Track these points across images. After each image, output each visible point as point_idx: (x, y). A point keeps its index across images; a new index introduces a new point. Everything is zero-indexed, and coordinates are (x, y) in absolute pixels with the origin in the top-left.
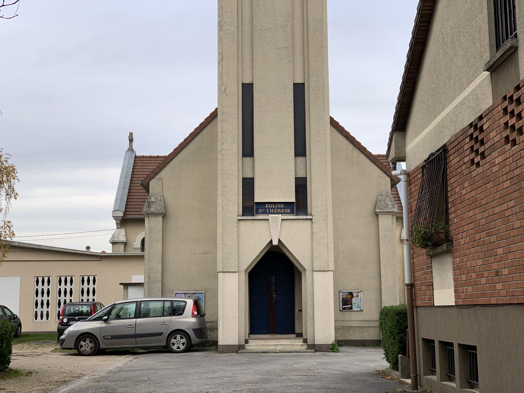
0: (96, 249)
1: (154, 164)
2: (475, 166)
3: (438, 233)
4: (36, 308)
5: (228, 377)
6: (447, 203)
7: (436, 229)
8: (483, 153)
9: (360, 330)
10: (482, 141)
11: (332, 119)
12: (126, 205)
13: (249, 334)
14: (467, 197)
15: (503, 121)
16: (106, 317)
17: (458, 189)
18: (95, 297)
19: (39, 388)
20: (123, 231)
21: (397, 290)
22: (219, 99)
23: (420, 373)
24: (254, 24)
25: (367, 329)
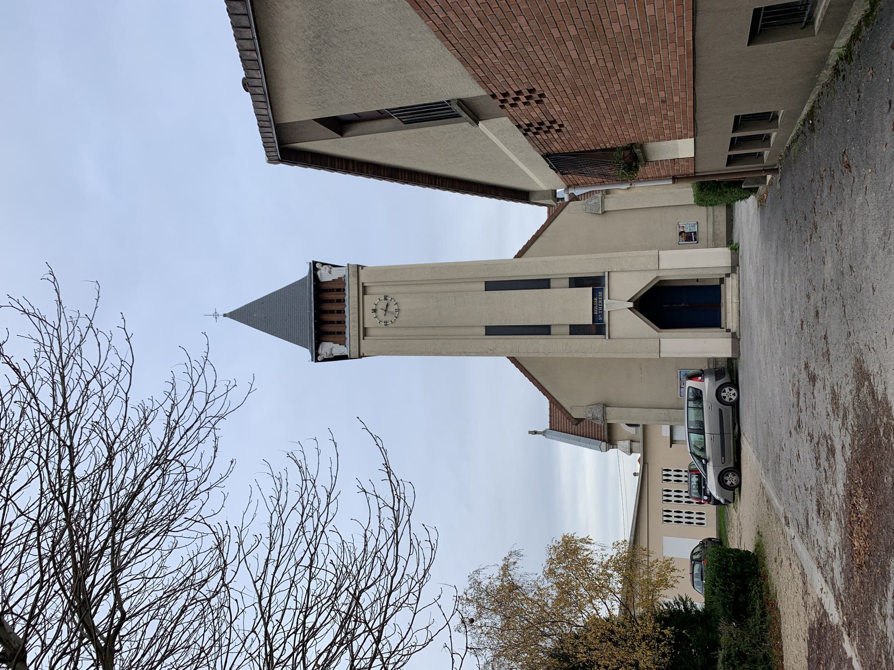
0: (638, 468)
1: (557, 413)
2: (562, 129)
3: (624, 158)
4: (671, 521)
5: (765, 348)
6: (596, 151)
7: (620, 159)
8: (551, 122)
9: (716, 224)
10: (539, 124)
11: (516, 257)
12: (595, 439)
13: (721, 328)
14: (590, 133)
15: (522, 107)
16: (703, 461)
17: (583, 142)
18: (683, 470)
19: (774, 526)
20: (620, 443)
21: (677, 191)
22: (500, 356)
23: (760, 167)
24: (435, 325)
25: (715, 217)
